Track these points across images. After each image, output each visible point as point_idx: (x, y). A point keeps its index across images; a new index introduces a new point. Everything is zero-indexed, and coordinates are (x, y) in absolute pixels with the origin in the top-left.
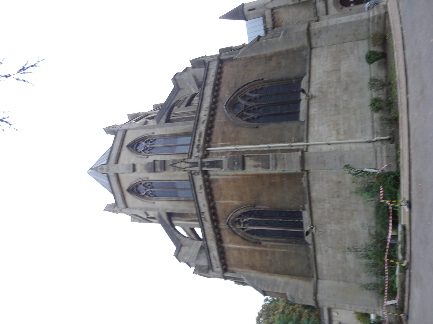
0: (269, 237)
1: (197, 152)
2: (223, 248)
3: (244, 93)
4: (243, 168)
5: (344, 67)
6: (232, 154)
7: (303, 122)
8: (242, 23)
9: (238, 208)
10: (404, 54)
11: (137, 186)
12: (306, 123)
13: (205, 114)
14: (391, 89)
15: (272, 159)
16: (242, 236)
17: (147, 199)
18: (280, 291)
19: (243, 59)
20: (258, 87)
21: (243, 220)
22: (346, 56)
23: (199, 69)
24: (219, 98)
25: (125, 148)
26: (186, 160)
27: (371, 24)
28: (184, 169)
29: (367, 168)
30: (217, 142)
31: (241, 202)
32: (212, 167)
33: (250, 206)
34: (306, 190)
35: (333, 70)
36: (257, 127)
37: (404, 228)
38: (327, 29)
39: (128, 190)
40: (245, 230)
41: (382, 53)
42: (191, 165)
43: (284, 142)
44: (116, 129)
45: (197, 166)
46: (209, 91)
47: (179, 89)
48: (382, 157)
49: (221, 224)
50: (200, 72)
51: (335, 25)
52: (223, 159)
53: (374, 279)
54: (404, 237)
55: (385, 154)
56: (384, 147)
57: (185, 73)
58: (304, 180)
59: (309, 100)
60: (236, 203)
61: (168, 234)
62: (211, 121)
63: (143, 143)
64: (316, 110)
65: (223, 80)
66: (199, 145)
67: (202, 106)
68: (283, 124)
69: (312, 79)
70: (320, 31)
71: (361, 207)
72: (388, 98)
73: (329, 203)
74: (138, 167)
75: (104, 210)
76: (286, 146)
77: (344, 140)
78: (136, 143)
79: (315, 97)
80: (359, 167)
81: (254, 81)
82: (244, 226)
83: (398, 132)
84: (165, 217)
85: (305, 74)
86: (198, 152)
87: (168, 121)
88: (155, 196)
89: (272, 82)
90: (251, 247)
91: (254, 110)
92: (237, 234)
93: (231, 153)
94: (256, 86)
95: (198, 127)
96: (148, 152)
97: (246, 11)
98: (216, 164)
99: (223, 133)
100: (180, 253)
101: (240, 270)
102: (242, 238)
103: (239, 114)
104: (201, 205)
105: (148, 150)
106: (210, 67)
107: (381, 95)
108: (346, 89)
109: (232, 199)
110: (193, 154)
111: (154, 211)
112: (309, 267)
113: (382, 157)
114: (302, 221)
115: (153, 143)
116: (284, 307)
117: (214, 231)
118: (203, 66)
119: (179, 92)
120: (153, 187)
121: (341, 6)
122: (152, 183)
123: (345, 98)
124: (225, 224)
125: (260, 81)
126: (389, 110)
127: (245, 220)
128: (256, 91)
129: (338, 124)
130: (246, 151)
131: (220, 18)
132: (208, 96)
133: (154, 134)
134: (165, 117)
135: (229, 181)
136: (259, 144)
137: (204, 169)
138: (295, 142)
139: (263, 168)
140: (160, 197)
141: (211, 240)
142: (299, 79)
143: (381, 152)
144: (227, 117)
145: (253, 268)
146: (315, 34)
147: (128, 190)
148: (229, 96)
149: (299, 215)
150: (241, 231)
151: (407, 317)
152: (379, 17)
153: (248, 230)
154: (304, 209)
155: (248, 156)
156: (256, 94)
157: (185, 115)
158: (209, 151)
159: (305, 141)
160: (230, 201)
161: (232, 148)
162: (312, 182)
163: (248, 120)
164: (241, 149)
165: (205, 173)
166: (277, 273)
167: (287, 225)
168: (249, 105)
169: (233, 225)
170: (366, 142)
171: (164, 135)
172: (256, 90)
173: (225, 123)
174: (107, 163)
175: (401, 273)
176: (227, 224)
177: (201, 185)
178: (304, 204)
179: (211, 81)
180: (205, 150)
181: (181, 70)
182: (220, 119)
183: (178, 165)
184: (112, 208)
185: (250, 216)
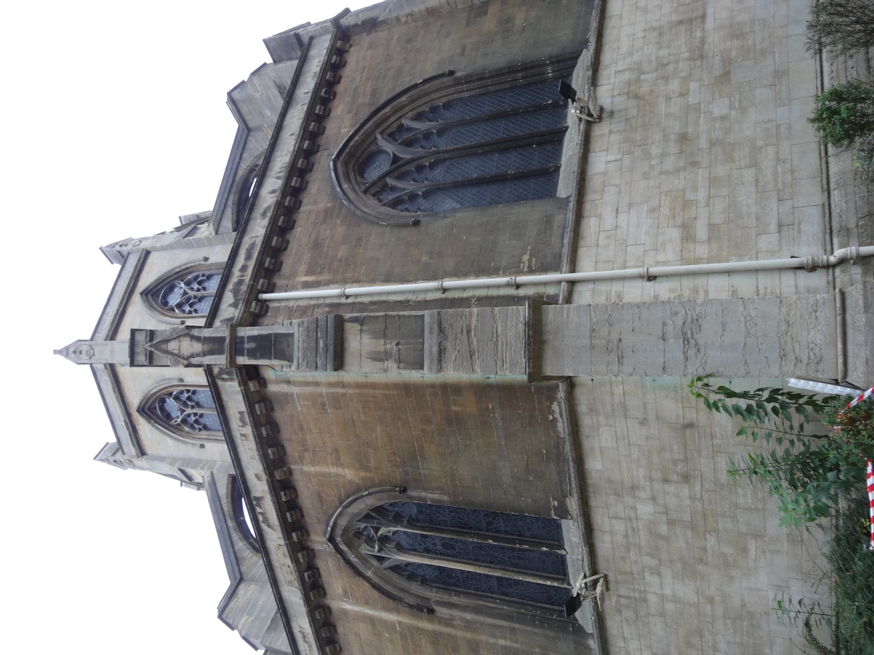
0: (458, 593)
1: (231, 305)
3: (395, 121)
4: (339, 363)
9: (355, 493)
11: (163, 401)
12: (572, 205)
13: (275, 188)
15: (431, 332)
16: (376, 580)
19: (403, 20)
20: (436, 99)
24: (322, 140)
25: (137, 298)
28: (187, 358)
29: (799, 378)
30: (294, 275)
32: (263, 357)
35: (681, 22)
36: (416, 223)
39: (141, 410)
40: (387, 564)
42: (207, 347)
44: (125, 250)
45: (221, 352)
47: (249, 130)
49: (313, 537)
58: (558, 409)
59: (589, 124)
60: (349, 474)
62: (286, 207)
63: (182, 285)
64: (611, 157)
65: (340, 88)
66: (240, 282)
68: (499, 210)
69: (607, 57)
73: (654, 499)
75: (95, 458)
76: (499, 286)
77: (709, 261)
81: (425, 81)
82: (380, 550)
85: (585, 44)
86: (235, 305)
89: (478, 80)
90: (406, 620)
93: (327, 309)
94: (433, 96)
95: (249, 228)
96: (187, 308)
99: (317, 245)
102: (375, 586)
106: (313, 52)
109: (338, 463)
114: (563, 552)
117: (295, 560)
119: (250, 138)
122: (194, 392)
123: (719, 108)
125: (445, 79)
127: (383, 531)
129: (687, 204)
130: (372, 303)
133: (210, 262)
136: (416, 280)
137: (242, 360)
138: (531, 271)
139: (402, 365)
141: (290, 583)
147: (141, 410)
148: (350, 132)
150: (376, 563)
153: (395, 564)
154: (564, 513)
158: (268, 303)
159: (565, 266)
160: (333, 470)
161: (332, 291)
162: (586, 421)
164: (356, 296)
165: (251, 374)
169: (349, 545)
170: (800, 268)
173: (327, 215)
174: (92, 339)
177: (241, 413)
178: (563, 496)
183: (173, 346)
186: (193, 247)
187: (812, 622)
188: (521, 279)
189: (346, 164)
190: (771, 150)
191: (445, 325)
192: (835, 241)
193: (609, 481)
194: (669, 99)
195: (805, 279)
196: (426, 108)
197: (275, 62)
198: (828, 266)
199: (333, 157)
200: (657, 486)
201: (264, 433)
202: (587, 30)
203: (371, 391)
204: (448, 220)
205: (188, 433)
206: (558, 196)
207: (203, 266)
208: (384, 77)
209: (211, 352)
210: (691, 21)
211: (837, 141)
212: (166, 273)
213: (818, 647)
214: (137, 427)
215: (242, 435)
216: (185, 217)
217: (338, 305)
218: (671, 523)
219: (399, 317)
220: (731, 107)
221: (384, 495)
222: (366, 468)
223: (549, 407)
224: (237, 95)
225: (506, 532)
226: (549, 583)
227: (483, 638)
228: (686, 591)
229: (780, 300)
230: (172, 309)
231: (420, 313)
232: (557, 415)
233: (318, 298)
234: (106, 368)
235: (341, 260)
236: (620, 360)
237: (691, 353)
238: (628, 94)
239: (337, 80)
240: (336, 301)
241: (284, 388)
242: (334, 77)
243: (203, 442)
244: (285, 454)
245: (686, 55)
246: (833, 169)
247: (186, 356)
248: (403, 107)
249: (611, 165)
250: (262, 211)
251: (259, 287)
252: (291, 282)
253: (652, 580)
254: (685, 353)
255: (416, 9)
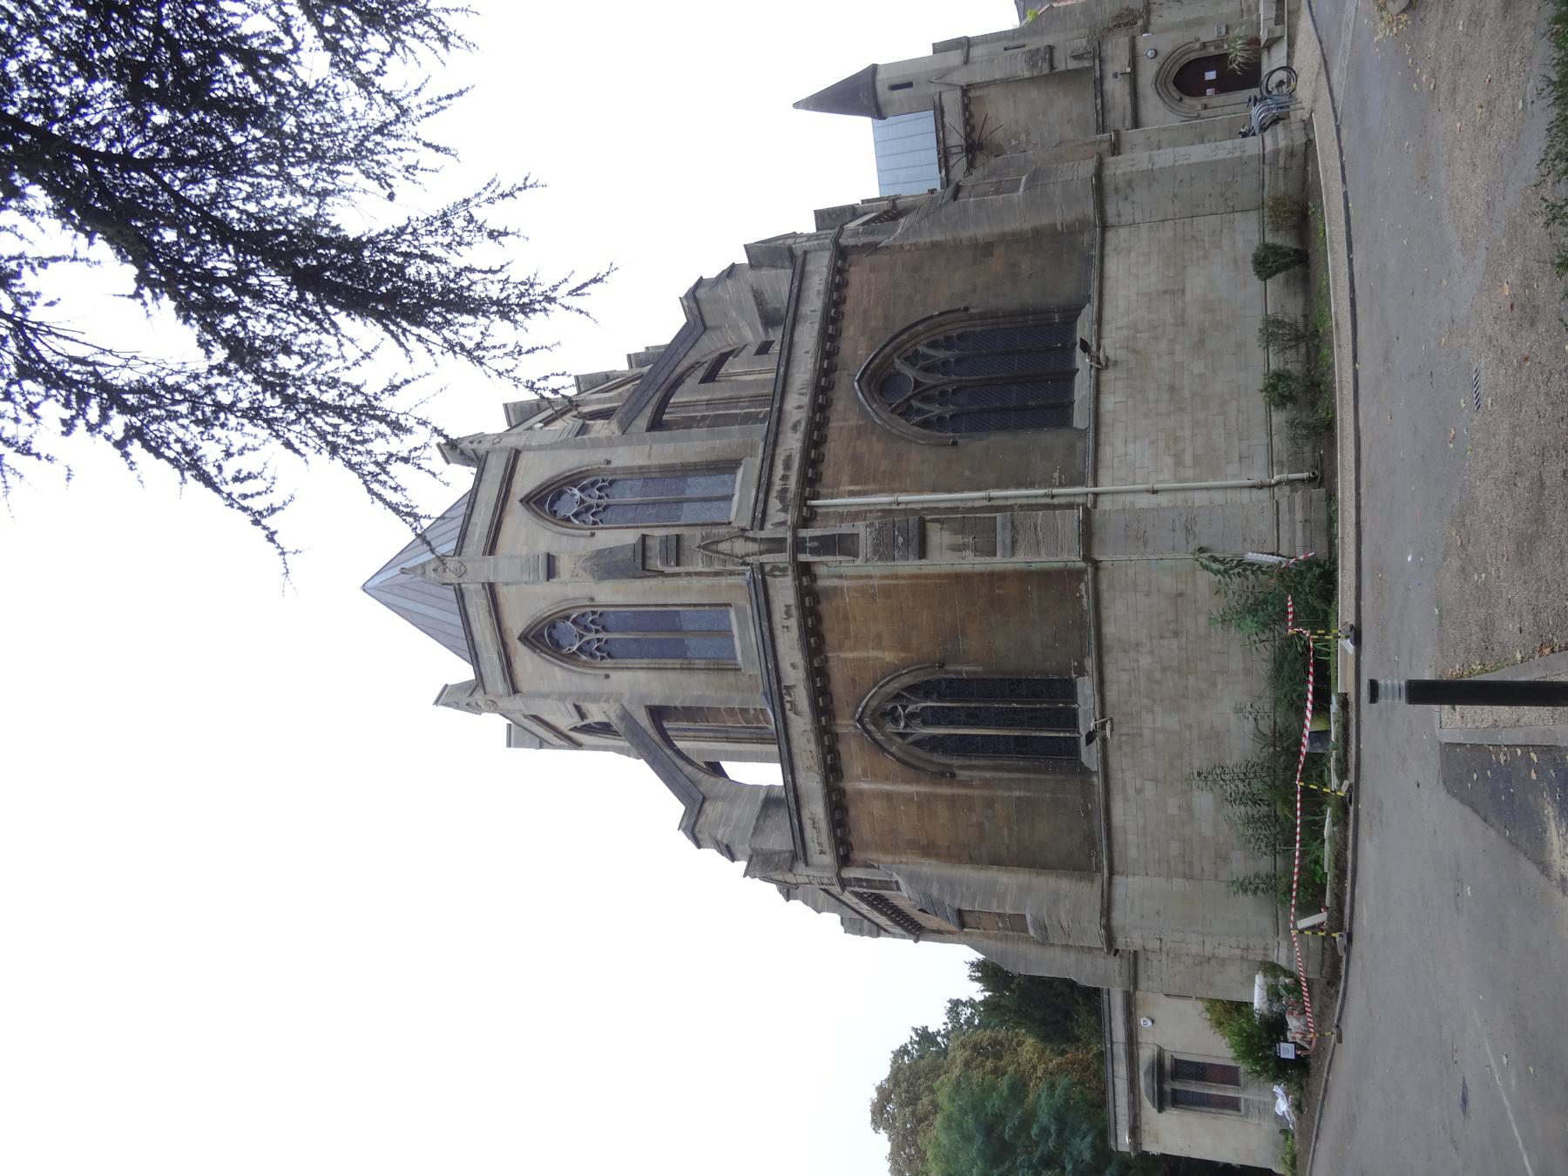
0: (977, 758)
2: (842, 793)
4: (922, 553)
5: (1196, 283)
6: (881, 517)
7: (1085, 431)
8: (861, 127)
9: (894, 671)
10: (1350, 260)
11: (553, 625)
12: (1091, 435)
14: (1318, 348)
15: (1004, 528)
16: (900, 754)
17: (585, 665)
18: (1009, 911)
21: (904, 708)
22: (1201, 253)
23: (773, 271)
24: (839, 359)
25: (514, 504)
26: (750, 534)
27: (1267, 169)
28: (742, 557)
29: (1253, 552)
30: (838, 484)
31: (903, 655)
33: (930, 667)
34: (1090, 619)
35: (1166, 292)
36: (955, 444)
37: (1344, 703)
38: (1150, 176)
39: (524, 638)
40: (910, 739)
41: (1296, 251)
42: (763, 547)
43: (1031, 485)
45: (782, 550)
46: (807, 337)
47: (705, 328)
48: (1293, 521)
49: (840, 721)
50: (778, 282)
51: (1173, 167)
52: (860, 528)
53: (1265, 864)
54: (1345, 727)
55: (1299, 516)
56: (1298, 496)
57: (729, 283)
59: (1098, 370)
60: (889, 656)
61: (655, 771)
62: (817, 423)
63: (576, 491)
65: (848, 308)
66: (784, 491)
67: (789, 380)
69: (1108, 314)
70: (1130, 183)
71: (1236, 663)
72: (1309, 371)
73: (1152, 652)
74: (564, 565)
75: (436, 702)
77: (1194, 481)
78: (551, 492)
79: (1116, 363)
80: (1229, 551)
81: (941, 314)
82: (906, 726)
83: (1333, 459)
84: (644, 720)
85: (1087, 299)
86: (785, 510)
87: (656, 424)
88: (610, 656)
89: (992, 318)
90: (924, 789)
91: (943, 397)
92: (884, 750)
93: (879, 514)
94: (948, 327)
95: (780, 441)
97: (882, 89)
98: (840, 545)
99: (855, 459)
100: (702, 820)
101: (889, 858)
102: (899, 760)
103: (899, 405)
104: (785, 665)
105: (594, 515)
106: (810, 268)
107: (1292, 362)
108: (1201, 343)
109: (879, 647)
110: (768, 518)
111: (607, 701)
112: (1090, 840)
113: (1293, 521)
114: (1076, 706)
115: (608, 491)
116: (967, 1064)
117: (819, 742)
118: (787, 263)
119: (704, 337)
120: (605, 629)
121: (1176, 94)
123: (1198, 367)
124: (852, 722)
125: (961, 314)
126: (1313, 404)
127: (910, 708)
128: (948, 343)
131: (797, 105)
132: (807, 352)
134: (648, 412)
135: (873, 595)
136: (962, 491)
137: (803, 558)
138: (1061, 485)
140: (621, 658)
141: (809, 769)
142: (1071, 313)
143: (1291, 510)
144: (866, 416)
145: (928, 850)
146: (1117, 190)
147: (524, 638)
149: (1067, 690)
150: (899, 740)
151: (1350, 938)
152: (1291, 154)
153: (918, 738)
154: (1081, 671)
155: (937, 521)
156: (948, 350)
157: (698, 408)
159: (1090, 483)
160: (873, 654)
163: (925, 424)
164: (907, 503)
165: (805, 570)
166: (997, 861)
167: (1034, 719)
168: (929, 380)
169: (875, 724)
171: (640, 467)
172: (948, 339)
175: (1335, 829)
176: (860, 720)
177: (788, 607)
178: (1082, 656)
179: (813, 309)
180: (806, 505)
181: (711, 272)
182: (843, 418)
183: (724, 547)
184: (451, 697)
185: (927, 696)
186: (585, 447)
187: (1259, 717)
188: (1056, 491)
189: (868, 384)
190: (1235, 403)
191: (1017, 523)
192: (1275, 470)
193: (1120, 641)
194: (1159, 356)
195: (1256, 494)
196: (941, 337)
197: (751, 265)
198: (1270, 486)
199: (857, 378)
200: (1155, 641)
201: (810, 623)
202: (1088, 287)
203: (923, 581)
204: (984, 442)
205: (585, 662)
206: (1075, 425)
207: (605, 470)
208: (895, 304)
209: (769, 551)
210: (1173, 292)
211: (1277, 406)
212: (553, 478)
213: (1314, 93)
214: (512, 660)
215: (784, 627)
216: (515, 404)
217: (890, 511)
218: (1164, 670)
219: (975, 518)
220: (1206, 367)
221: (922, 672)
222: (905, 649)
223: (1078, 587)
224: (701, 294)
225: (1027, 697)
226: (1062, 735)
227: (999, 793)
228: (1171, 722)
229: (1243, 506)
230: (568, 520)
231: (993, 515)
232: (1084, 593)
233: (869, 505)
234: (484, 588)
235: (884, 472)
236: (1146, 544)
237: (1191, 538)
238: (1127, 348)
239: (842, 300)
240: (888, 507)
241: (836, 582)
242: (840, 297)
243: (607, 672)
244: (824, 643)
245: (1171, 321)
246: (1274, 421)
247: (739, 555)
248: (919, 335)
249: (1118, 406)
250: (790, 425)
251: (807, 495)
252: (835, 490)
253: (1147, 716)
254: (1187, 539)
255: (921, 241)
